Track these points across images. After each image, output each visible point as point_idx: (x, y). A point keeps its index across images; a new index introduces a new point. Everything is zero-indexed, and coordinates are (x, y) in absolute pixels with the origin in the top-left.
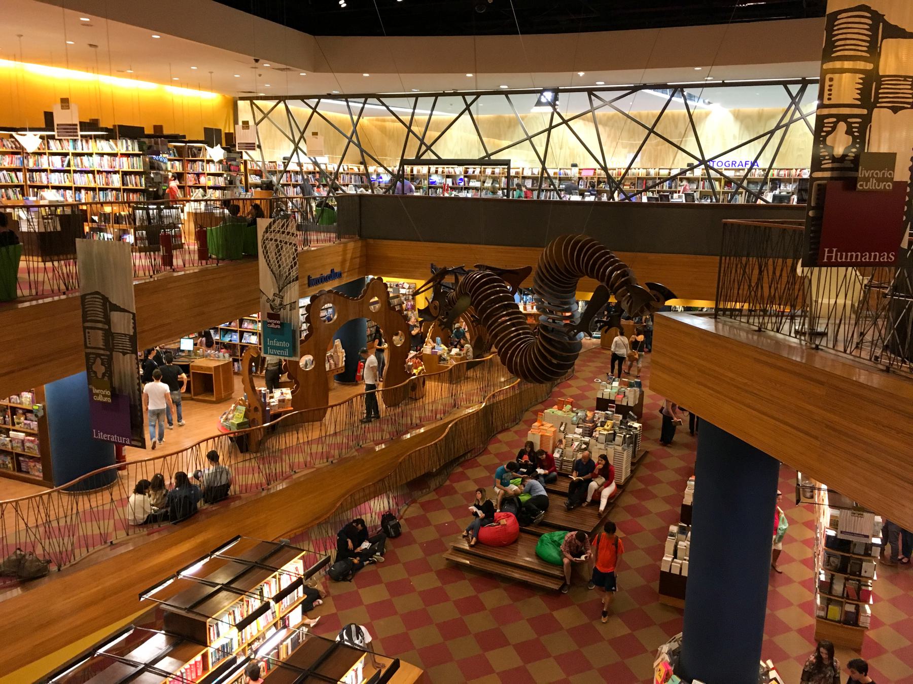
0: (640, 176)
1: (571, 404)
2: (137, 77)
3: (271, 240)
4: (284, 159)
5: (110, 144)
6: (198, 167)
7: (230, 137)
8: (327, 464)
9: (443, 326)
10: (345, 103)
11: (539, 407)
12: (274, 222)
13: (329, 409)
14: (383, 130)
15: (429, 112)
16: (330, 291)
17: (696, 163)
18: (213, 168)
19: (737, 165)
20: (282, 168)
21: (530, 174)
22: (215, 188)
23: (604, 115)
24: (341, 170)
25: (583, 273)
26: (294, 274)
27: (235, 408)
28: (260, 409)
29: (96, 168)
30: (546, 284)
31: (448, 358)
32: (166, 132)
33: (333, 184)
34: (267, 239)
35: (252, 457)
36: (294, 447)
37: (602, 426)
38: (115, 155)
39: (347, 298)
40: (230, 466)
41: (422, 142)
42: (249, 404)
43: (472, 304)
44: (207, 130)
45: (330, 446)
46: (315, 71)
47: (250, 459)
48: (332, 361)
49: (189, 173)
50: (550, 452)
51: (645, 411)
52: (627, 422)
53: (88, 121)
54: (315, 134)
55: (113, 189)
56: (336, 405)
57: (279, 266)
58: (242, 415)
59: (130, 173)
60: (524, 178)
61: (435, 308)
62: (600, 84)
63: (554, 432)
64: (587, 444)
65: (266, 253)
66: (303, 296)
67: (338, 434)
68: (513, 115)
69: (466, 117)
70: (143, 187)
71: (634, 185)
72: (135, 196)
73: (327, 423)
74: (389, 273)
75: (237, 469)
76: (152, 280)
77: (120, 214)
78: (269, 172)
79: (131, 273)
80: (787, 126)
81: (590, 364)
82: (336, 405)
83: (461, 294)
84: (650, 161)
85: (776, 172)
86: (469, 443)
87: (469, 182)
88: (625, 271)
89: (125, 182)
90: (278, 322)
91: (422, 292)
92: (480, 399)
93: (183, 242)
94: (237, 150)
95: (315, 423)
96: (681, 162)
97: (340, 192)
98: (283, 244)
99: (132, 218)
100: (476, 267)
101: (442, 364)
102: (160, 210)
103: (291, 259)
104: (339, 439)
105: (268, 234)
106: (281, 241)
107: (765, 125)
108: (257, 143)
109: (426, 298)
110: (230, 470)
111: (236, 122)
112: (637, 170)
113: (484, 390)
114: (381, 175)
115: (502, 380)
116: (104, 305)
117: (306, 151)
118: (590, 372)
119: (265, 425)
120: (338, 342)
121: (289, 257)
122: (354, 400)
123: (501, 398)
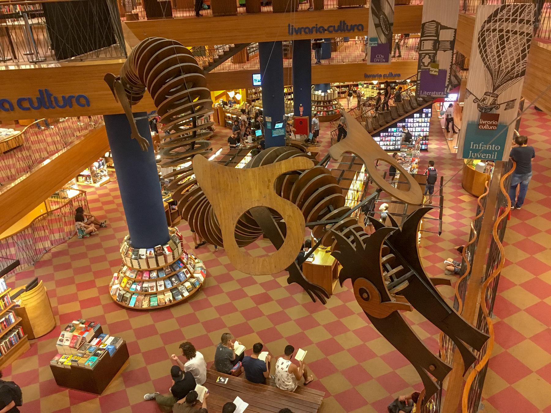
26: (519, 68)
34: (487, 30)
57: (500, 61)
98: (510, 34)
116: (437, 27)
121: (517, 49)
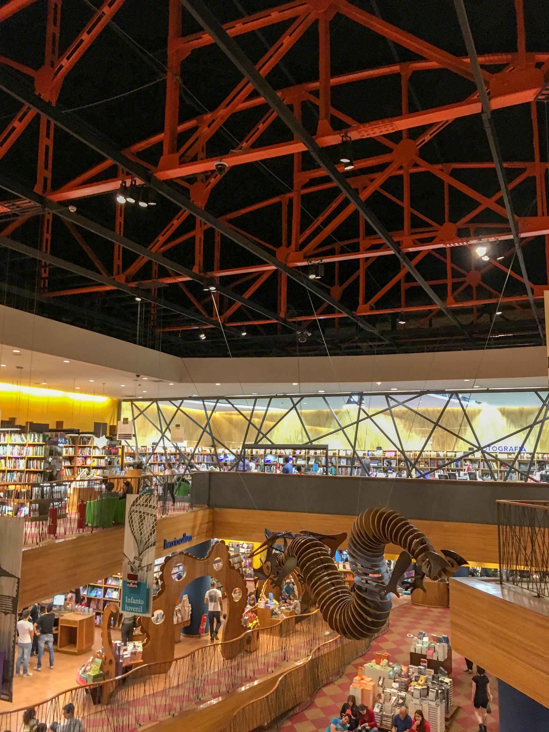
0: (432, 457)
1: (388, 658)
2: (49, 387)
3: (136, 511)
4: (153, 444)
5: (21, 437)
6: (86, 452)
7: (113, 429)
8: (169, 717)
9: (274, 585)
10: (202, 403)
11: (360, 660)
12: (140, 497)
13: (174, 662)
14: (230, 421)
15: (266, 408)
16: (181, 553)
17: (475, 449)
18: (97, 453)
19: (508, 450)
20: (151, 451)
21: (344, 455)
22: (97, 468)
23: (400, 411)
24: (197, 452)
25: (388, 540)
26: (152, 540)
27: (93, 659)
28: (114, 661)
29: (8, 455)
30: (359, 550)
31: (280, 612)
32: (65, 427)
33: (189, 463)
34: (133, 511)
35: (103, 709)
36: (141, 700)
37: (417, 681)
38: (24, 445)
39: (196, 558)
40: (83, 718)
41: (259, 431)
42: (105, 657)
43: (298, 565)
44: (96, 424)
45: (172, 698)
46: (180, 382)
47: (101, 711)
48: (179, 615)
49: (78, 457)
50: (370, 707)
51: (454, 665)
52: (438, 678)
53: (8, 420)
54: (178, 426)
55: (18, 471)
56: (180, 659)
57: (141, 534)
58: (99, 667)
59: (33, 459)
60: (340, 457)
61: (268, 567)
62: (394, 390)
63: (374, 686)
64: (404, 699)
65: (131, 522)
66: (158, 556)
67: (180, 687)
68: (329, 410)
69: (294, 411)
70: (42, 469)
71: (428, 464)
72: (35, 476)
73: (171, 675)
74: (229, 536)
75: (89, 721)
76: (38, 546)
77: (21, 491)
78: (140, 454)
79: (22, 541)
80: (542, 422)
81: (403, 619)
82: (180, 659)
83: (289, 556)
84: (439, 445)
85: (540, 456)
86: (297, 696)
87: (296, 461)
88: (423, 539)
89: (29, 466)
90: (136, 582)
91: (257, 554)
92: (307, 651)
93: (67, 512)
94: (118, 439)
95: (161, 675)
96: (461, 448)
97: (195, 469)
98: (145, 515)
99: (29, 495)
100: (301, 532)
101: (274, 618)
102: (52, 487)
103: (151, 527)
104: (181, 692)
105: (135, 507)
106: (144, 513)
107: (527, 419)
108: (134, 433)
109: (260, 559)
110: (83, 723)
111: (119, 419)
112: (429, 453)
113: (310, 643)
114: (228, 455)
115: (327, 633)
117: (170, 439)
118: (404, 627)
119: (117, 678)
120: (185, 597)
121: (150, 525)
122: (196, 653)
123: (326, 651)
